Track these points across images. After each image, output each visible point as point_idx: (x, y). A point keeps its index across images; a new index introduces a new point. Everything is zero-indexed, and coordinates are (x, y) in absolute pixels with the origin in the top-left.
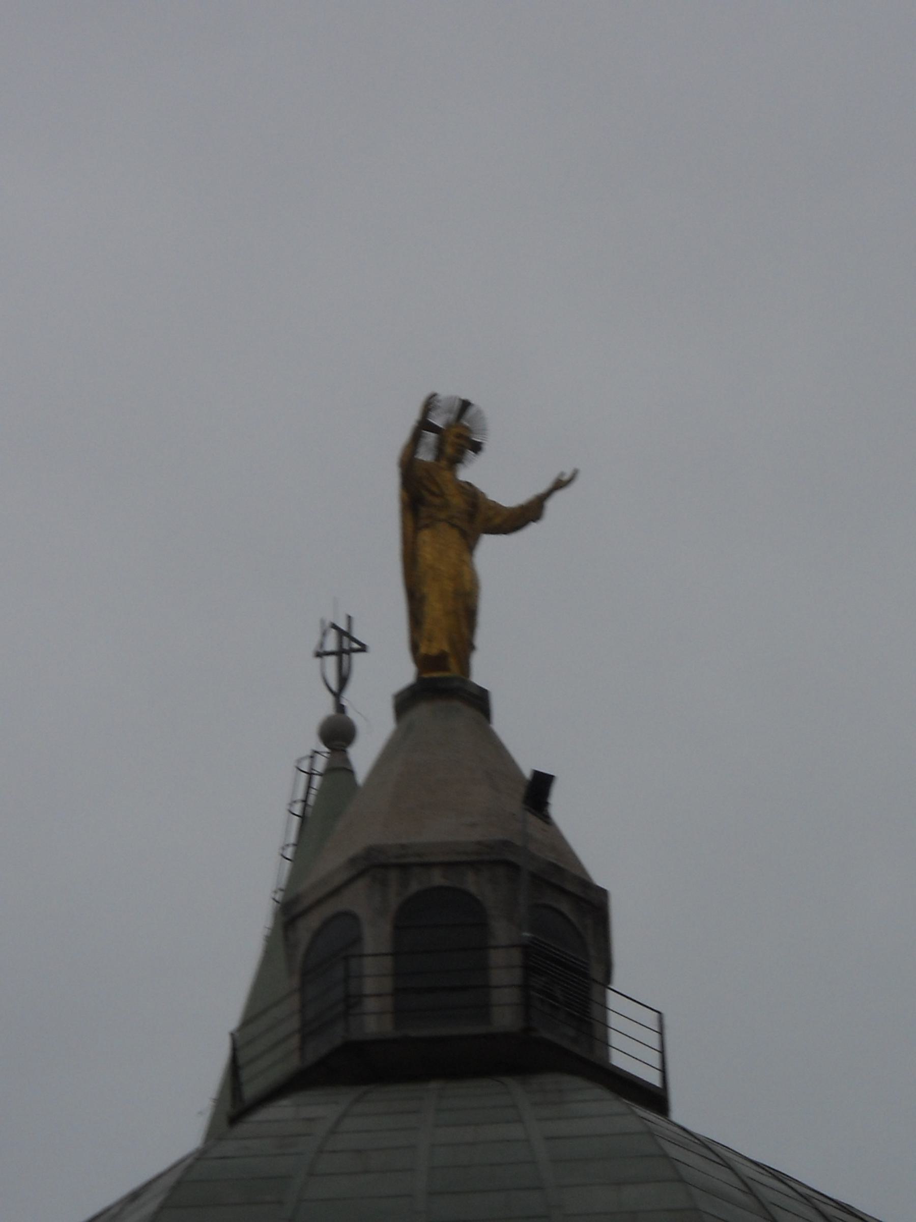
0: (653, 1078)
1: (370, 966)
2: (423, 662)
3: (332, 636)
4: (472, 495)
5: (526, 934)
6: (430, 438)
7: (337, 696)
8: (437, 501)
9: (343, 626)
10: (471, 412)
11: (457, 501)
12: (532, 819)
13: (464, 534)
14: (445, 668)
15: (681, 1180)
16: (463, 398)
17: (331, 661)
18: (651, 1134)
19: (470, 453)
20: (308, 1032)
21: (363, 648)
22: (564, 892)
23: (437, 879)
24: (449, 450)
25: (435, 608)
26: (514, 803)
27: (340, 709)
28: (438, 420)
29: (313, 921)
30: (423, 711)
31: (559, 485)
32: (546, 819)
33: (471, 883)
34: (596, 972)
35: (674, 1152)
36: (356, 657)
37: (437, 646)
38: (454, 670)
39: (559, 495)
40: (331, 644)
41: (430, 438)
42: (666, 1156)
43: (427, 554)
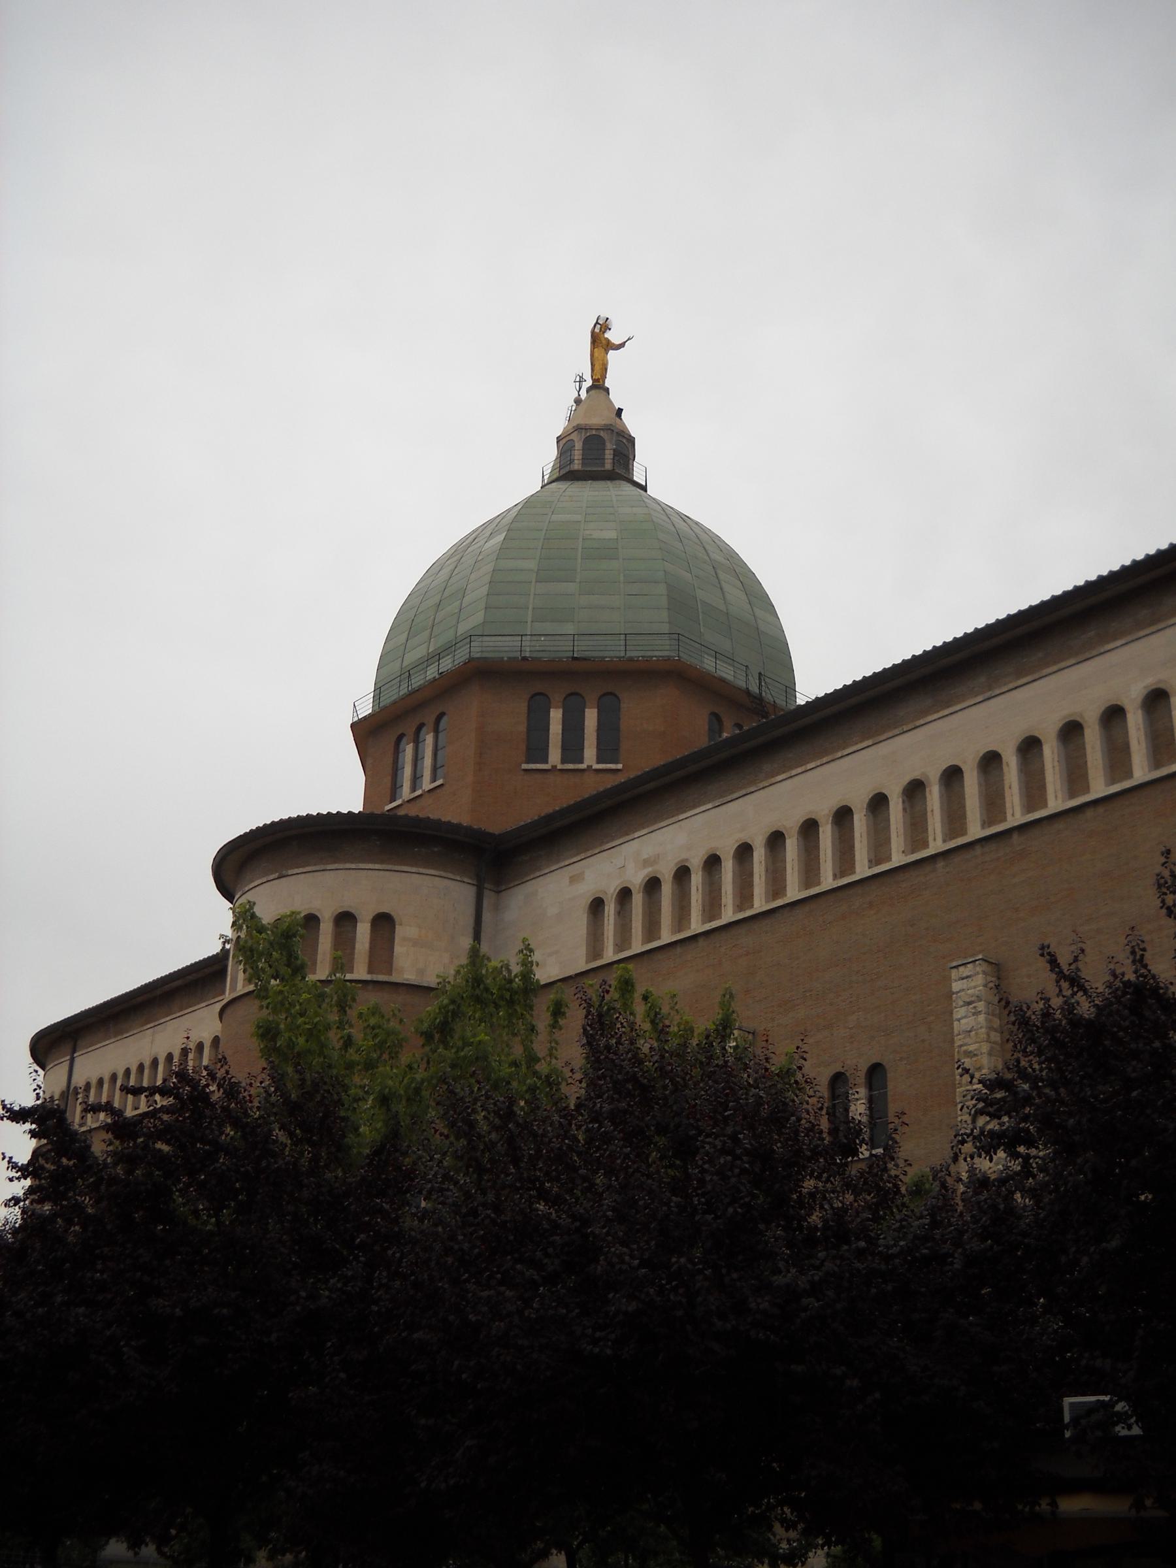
0: (644, 484)
1: (576, 452)
2: (594, 380)
3: (578, 377)
4: (608, 341)
5: (614, 447)
6: (598, 326)
7: (579, 392)
8: (599, 341)
9: (581, 375)
10: (608, 321)
11: (604, 342)
12: (617, 419)
13: (605, 350)
14: (599, 382)
15: (647, 507)
16: (632, 423)
17: (578, 384)
18: (641, 496)
19: (608, 331)
20: (561, 468)
21: (585, 381)
22: (624, 436)
23: (594, 432)
24: (603, 329)
25: (597, 367)
26: (614, 415)
27: (579, 395)
28: (601, 322)
29: (564, 441)
30: (592, 392)
31: (629, 339)
32: (621, 419)
33: (602, 434)
34: (631, 457)
35: (646, 500)
36: (583, 383)
37: (598, 380)
38: (601, 382)
39: (629, 341)
40: (578, 379)
41: (598, 326)
42: (644, 501)
43: (596, 354)
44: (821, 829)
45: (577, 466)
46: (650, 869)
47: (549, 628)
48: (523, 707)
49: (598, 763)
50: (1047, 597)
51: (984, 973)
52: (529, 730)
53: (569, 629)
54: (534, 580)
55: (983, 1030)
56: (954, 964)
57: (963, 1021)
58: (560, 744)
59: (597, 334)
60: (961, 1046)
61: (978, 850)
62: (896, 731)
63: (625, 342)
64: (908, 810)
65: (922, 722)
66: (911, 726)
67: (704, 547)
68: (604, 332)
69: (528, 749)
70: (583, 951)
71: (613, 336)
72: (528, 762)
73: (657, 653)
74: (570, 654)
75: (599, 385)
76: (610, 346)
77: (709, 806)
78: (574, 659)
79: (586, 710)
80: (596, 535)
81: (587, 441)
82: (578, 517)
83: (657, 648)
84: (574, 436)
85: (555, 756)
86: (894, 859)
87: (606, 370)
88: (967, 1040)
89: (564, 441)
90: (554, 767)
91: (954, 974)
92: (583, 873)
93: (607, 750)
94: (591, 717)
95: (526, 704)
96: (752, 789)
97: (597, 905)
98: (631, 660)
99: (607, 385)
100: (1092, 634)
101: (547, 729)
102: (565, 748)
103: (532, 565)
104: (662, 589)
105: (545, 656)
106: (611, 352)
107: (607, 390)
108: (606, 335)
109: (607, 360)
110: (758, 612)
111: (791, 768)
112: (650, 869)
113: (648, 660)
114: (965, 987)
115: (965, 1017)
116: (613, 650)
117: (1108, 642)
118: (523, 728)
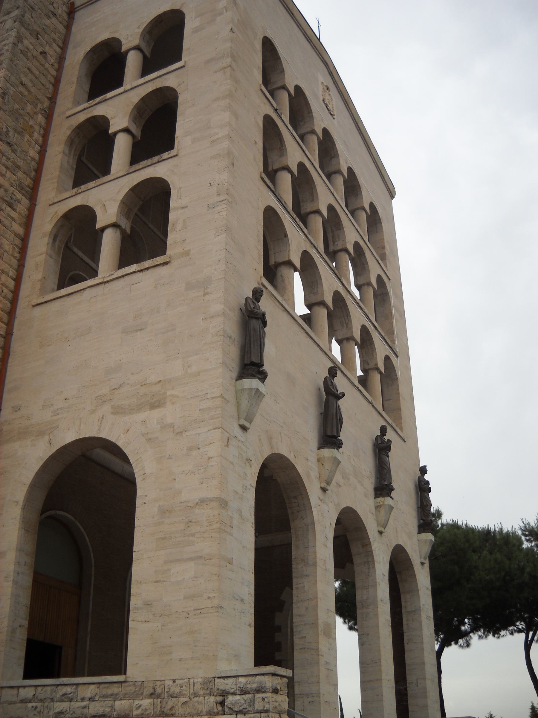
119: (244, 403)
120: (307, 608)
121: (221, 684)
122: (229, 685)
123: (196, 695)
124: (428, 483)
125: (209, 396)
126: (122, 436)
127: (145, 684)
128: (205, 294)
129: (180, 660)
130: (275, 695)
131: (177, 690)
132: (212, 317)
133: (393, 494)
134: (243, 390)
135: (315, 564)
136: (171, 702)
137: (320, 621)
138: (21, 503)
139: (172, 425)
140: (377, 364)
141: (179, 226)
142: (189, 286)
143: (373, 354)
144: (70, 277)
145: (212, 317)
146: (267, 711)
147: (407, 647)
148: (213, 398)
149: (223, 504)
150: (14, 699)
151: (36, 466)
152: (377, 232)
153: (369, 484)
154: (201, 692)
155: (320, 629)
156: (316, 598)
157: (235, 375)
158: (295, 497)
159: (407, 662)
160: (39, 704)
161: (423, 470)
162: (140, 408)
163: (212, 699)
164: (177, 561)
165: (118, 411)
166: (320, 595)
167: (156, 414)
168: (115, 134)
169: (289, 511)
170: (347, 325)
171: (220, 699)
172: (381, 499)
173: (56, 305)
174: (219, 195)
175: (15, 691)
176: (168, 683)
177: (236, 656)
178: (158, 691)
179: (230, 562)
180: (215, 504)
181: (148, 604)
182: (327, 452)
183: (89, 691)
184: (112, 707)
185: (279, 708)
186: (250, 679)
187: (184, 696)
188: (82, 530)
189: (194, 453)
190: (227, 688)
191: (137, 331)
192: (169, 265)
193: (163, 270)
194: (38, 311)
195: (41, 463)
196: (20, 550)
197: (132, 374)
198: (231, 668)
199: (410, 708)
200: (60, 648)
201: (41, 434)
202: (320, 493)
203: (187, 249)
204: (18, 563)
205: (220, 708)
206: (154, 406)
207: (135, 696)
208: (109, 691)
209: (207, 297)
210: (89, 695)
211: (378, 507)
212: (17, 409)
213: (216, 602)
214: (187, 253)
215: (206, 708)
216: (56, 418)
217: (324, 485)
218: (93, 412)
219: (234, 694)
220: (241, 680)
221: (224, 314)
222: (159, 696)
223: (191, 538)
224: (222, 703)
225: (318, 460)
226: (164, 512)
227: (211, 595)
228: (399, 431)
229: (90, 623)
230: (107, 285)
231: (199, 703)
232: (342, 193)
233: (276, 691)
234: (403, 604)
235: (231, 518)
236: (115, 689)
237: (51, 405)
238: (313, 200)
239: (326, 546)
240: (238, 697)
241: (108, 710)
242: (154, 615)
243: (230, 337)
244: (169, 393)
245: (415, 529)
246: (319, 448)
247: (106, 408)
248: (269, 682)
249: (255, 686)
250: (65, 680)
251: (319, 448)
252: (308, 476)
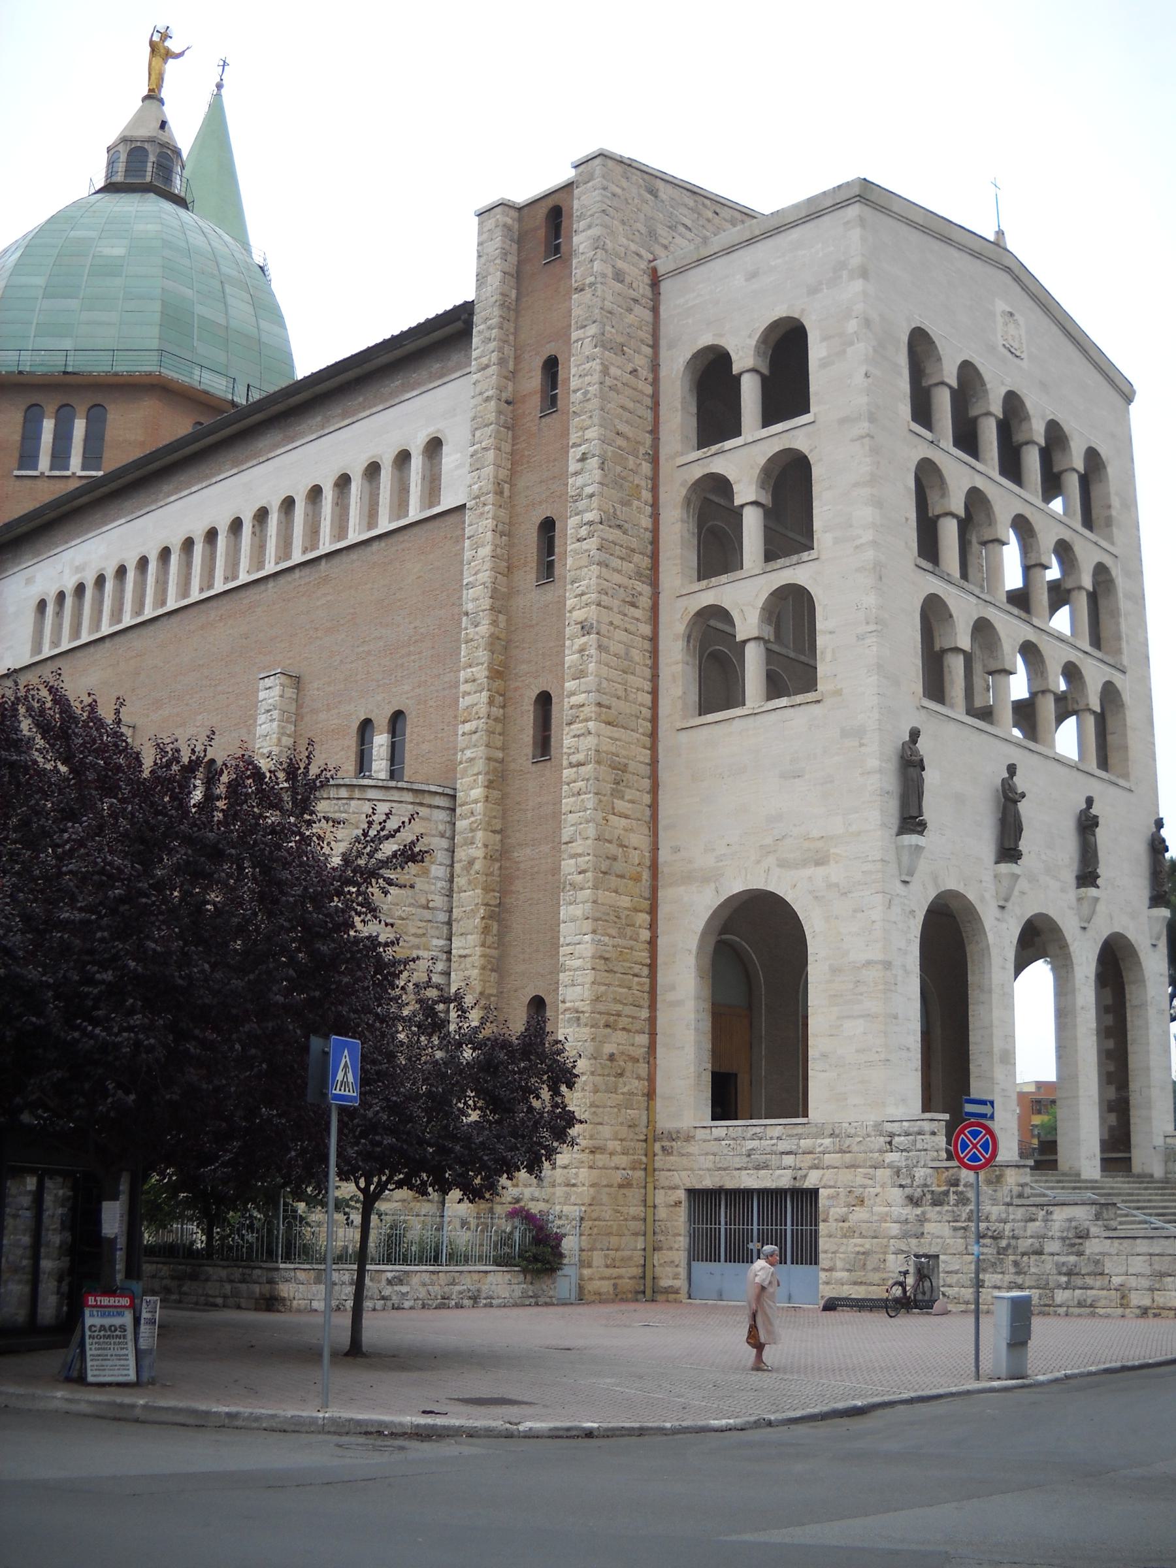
11: (163, 51)
23: (139, 144)
29: (112, 152)
30: (147, 102)
33: (146, 146)
43: (153, 63)
44: (195, 547)
45: (119, 178)
46: (79, 575)
47: (50, 343)
48: (19, 417)
49: (83, 469)
50: (388, 337)
51: (281, 685)
52: (23, 438)
53: (68, 344)
54: (40, 297)
55: (275, 736)
56: (262, 676)
57: (263, 726)
58: (50, 452)
59: (157, 42)
60: (259, 748)
61: (297, 574)
62: (255, 462)
63: (184, 52)
64: (258, 534)
65: (273, 455)
66: (264, 458)
67: (217, 262)
68: (164, 41)
69: (21, 457)
70: (28, 647)
71: (173, 45)
72: (19, 469)
73: (140, 369)
74: (62, 369)
75: (153, 96)
76: (168, 55)
77: (123, 521)
78: (65, 373)
79: (76, 421)
80: (107, 251)
81: (131, 153)
82: (94, 234)
83: (143, 363)
84: (121, 148)
85: (44, 463)
86: (241, 577)
87: (162, 79)
88: (265, 744)
89: (112, 152)
90: (42, 473)
91: (262, 684)
92: (35, 576)
93: (92, 457)
94: (79, 427)
95: (23, 414)
96: (154, 507)
97: (42, 605)
98: (116, 374)
99: (162, 95)
100: (397, 383)
101: (38, 438)
102: (54, 456)
103: (40, 281)
104: (157, 306)
105: (40, 370)
106: (170, 61)
107: (162, 101)
108: (166, 44)
109: (164, 70)
110: (264, 325)
111: (181, 490)
112: (79, 575)
113: (130, 374)
114: (267, 696)
115: (264, 723)
116: (99, 365)
117: (408, 392)
118: (17, 437)
119: (905, 859)
120: (983, 1037)
121: (889, 1127)
122: (895, 1128)
123: (868, 1136)
124: (1163, 841)
125: (870, 859)
126: (790, 891)
127: (825, 1126)
128: (861, 745)
129: (855, 1106)
130: (933, 1137)
131: (853, 1131)
132: (869, 773)
133: (1099, 881)
134: (903, 847)
135: (990, 991)
136: (848, 1141)
137: (996, 1050)
138: (694, 951)
139: (837, 885)
140: (1088, 705)
141: (829, 657)
142: (845, 734)
143: (1083, 690)
144: (709, 654)
145: (869, 773)
146: (926, 1150)
147: (1130, 1049)
148: (874, 861)
149: (887, 965)
150: (709, 1138)
151: (705, 915)
152: (1101, 482)
153: (1069, 875)
154: (873, 1133)
155: (996, 1058)
156: (991, 1026)
157: (895, 829)
158: (969, 922)
159: (1131, 1066)
160: (731, 1142)
161: (1159, 824)
162: (804, 863)
163: (882, 1139)
164: (848, 1017)
165: (783, 864)
166: (996, 1022)
167: (820, 871)
168: (740, 374)
169: (964, 935)
170: (1042, 673)
171: (888, 1139)
172: (1083, 889)
173: (705, 731)
174: (868, 623)
175: (708, 1131)
176: (845, 1125)
177: (903, 1100)
178: (837, 1132)
179: (896, 1017)
180: (880, 967)
181: (824, 1056)
182: (1004, 868)
183: (777, 1132)
184: (798, 1145)
185: (937, 1147)
186: (912, 1123)
187: (859, 1136)
188: (747, 947)
189: (859, 915)
190: (894, 1130)
191: (794, 777)
192: (821, 704)
193: (816, 709)
194: (684, 737)
195: (711, 912)
196: (697, 998)
197: (795, 825)
198: (898, 1112)
199: (1132, 1121)
200: (736, 1075)
201: (706, 880)
202: (996, 912)
203: (839, 687)
204: (697, 1011)
205: (888, 1147)
206: (819, 863)
207: (820, 1134)
208: (795, 1132)
209: (863, 749)
210: (776, 1134)
211: (1080, 899)
212: (676, 850)
213: (883, 1056)
214: (838, 693)
215: (877, 1147)
216: (721, 864)
217: (1002, 903)
218: (758, 862)
219: (899, 1135)
220: (905, 1124)
221: (880, 771)
222: (837, 1136)
223: (860, 997)
224: (890, 1143)
225: (995, 876)
226: (835, 971)
227: (879, 1050)
228: (1122, 782)
229: (763, 1047)
230: (758, 716)
231: (871, 1142)
232: (1036, 484)
233: (933, 1133)
234: (1128, 997)
235: (896, 976)
236: (799, 1130)
237: (714, 850)
238: (990, 525)
239: (1004, 968)
240: (903, 1138)
241: (794, 1147)
242: (830, 1065)
243: (888, 793)
244: (832, 851)
245: (1146, 902)
246: (997, 863)
247: (771, 860)
248: (927, 1126)
249: (916, 1129)
250: (754, 1122)
251: (997, 863)
252: (982, 899)
